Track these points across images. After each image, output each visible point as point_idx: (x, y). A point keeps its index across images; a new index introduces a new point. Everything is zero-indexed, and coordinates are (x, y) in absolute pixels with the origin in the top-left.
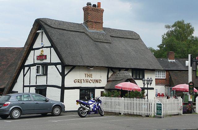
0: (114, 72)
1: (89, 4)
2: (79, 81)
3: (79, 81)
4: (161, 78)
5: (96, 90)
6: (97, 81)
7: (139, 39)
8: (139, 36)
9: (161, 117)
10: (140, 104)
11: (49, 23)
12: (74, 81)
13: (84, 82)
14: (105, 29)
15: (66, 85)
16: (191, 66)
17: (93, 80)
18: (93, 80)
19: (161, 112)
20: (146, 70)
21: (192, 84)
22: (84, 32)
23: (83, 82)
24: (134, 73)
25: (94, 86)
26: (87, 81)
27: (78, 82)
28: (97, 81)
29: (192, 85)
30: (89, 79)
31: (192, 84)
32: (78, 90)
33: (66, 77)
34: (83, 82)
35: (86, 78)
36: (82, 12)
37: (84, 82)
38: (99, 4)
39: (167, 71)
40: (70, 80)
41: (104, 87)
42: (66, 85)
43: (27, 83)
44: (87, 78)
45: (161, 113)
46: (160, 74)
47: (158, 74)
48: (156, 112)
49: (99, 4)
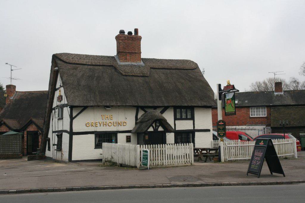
0: (146, 112)
1: (122, 32)
2: (93, 124)
3: (93, 124)
4: (261, 116)
5: (120, 136)
6: (119, 124)
7: (195, 70)
8: (196, 64)
9: (147, 169)
10: (225, 149)
11: (64, 58)
12: (86, 125)
13: (100, 126)
14: (145, 60)
15: (75, 130)
16: (62, 96)
17: (114, 122)
18: (114, 122)
19: (147, 161)
20: (196, 108)
21: (223, 123)
22: (112, 66)
23: (98, 125)
24: (188, 113)
25: (116, 130)
26: (105, 125)
27: (92, 126)
28: (119, 124)
29: (222, 125)
30: (108, 121)
31: (223, 123)
32: (93, 136)
33: (74, 121)
34: (98, 125)
35: (102, 121)
36: (115, 42)
37: (100, 126)
38: (136, 31)
39: (268, 107)
40: (79, 125)
41: (131, 130)
42: (75, 130)
43: (54, 130)
44: (105, 121)
45: (147, 163)
46: (260, 111)
47: (257, 111)
48: (142, 161)
49: (136, 31)
